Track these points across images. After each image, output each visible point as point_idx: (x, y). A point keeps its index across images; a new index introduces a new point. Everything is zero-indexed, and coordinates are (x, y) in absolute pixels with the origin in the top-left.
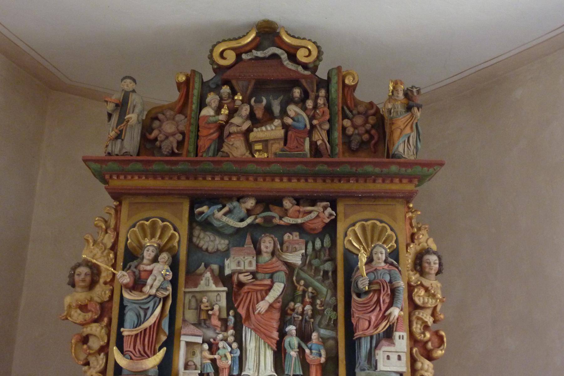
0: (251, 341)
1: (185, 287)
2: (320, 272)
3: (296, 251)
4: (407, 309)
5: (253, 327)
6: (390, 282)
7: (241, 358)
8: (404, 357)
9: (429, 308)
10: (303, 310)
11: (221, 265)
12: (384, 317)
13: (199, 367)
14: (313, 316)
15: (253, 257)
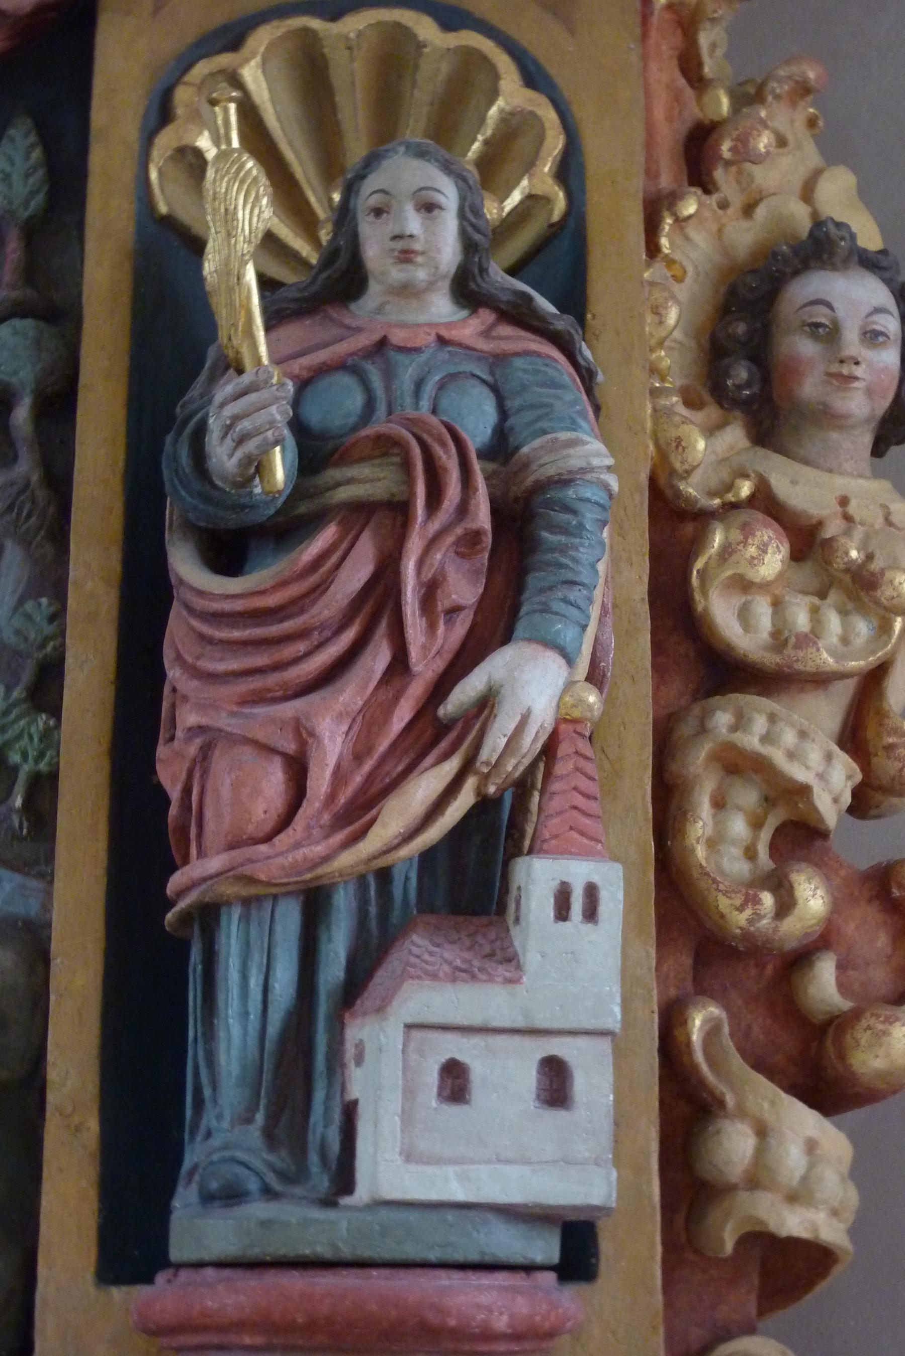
4: (646, 685)
6: (501, 447)
8: (594, 1080)
9: (820, 680)
12: (430, 733)
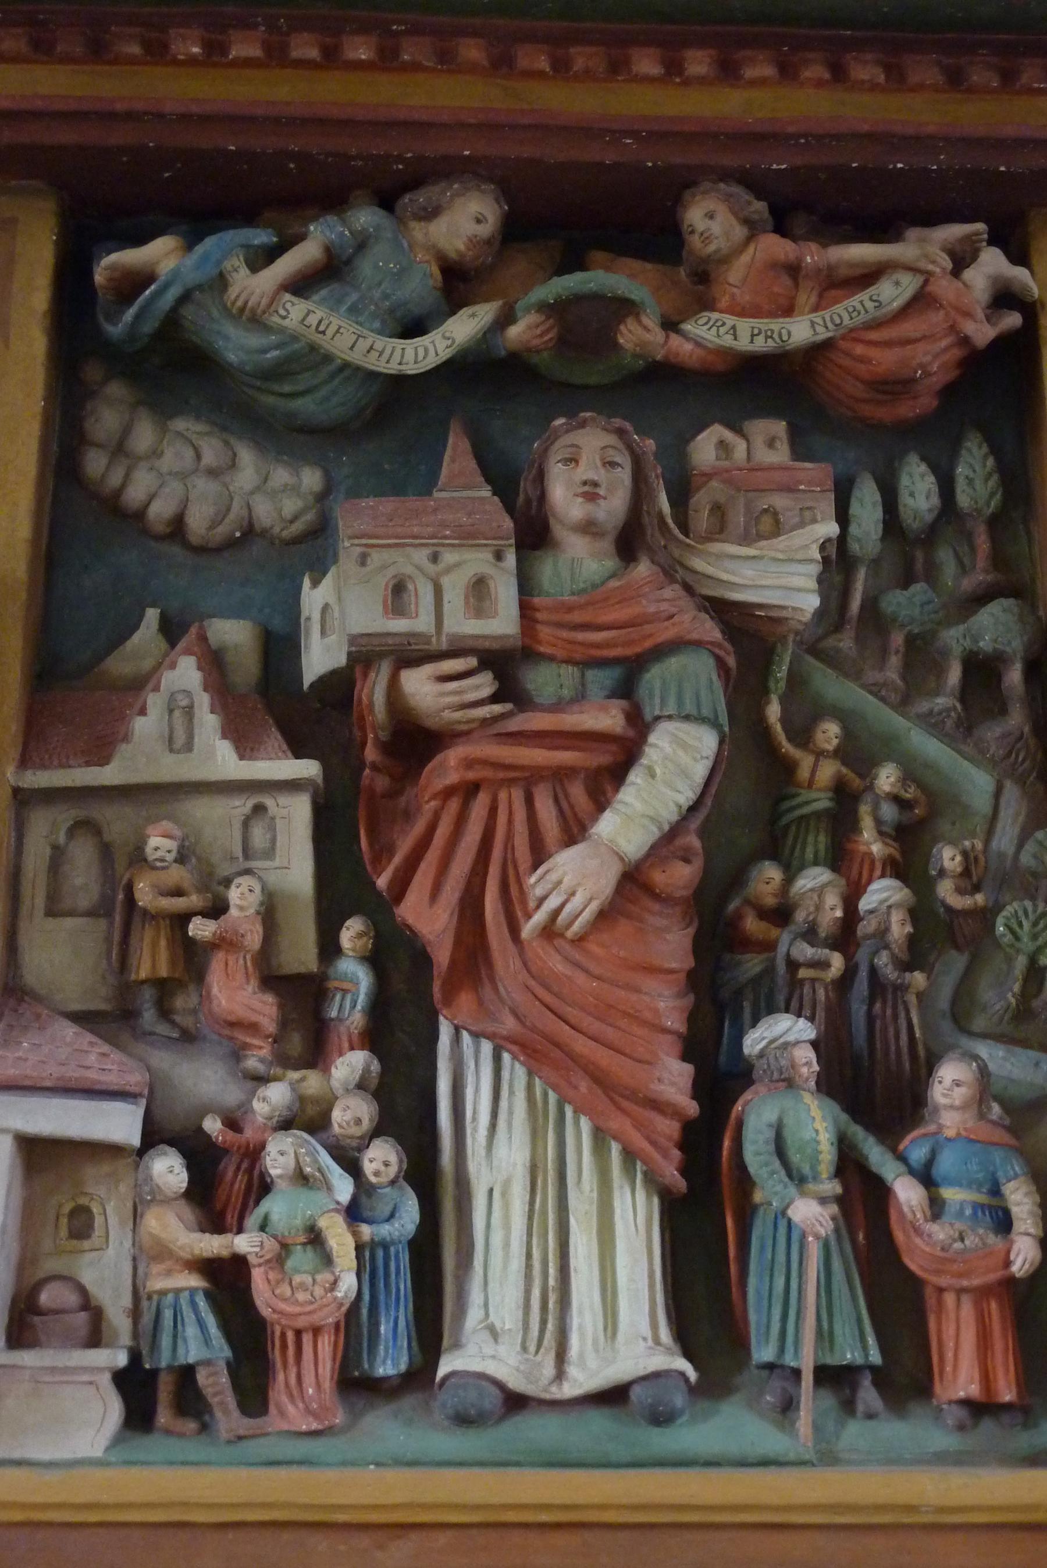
0: (499, 1129)
1: (24, 762)
2: (940, 670)
3: (777, 530)
5: (509, 1024)
7: (425, 1248)
10: (851, 916)
11: (278, 624)
13: (119, 1320)
14: (916, 955)
15: (499, 556)
